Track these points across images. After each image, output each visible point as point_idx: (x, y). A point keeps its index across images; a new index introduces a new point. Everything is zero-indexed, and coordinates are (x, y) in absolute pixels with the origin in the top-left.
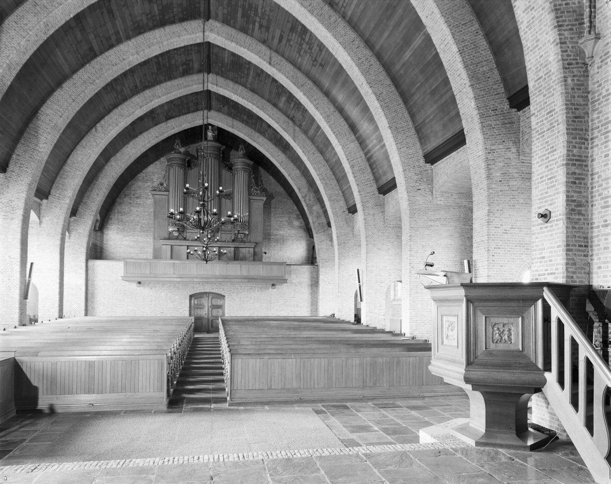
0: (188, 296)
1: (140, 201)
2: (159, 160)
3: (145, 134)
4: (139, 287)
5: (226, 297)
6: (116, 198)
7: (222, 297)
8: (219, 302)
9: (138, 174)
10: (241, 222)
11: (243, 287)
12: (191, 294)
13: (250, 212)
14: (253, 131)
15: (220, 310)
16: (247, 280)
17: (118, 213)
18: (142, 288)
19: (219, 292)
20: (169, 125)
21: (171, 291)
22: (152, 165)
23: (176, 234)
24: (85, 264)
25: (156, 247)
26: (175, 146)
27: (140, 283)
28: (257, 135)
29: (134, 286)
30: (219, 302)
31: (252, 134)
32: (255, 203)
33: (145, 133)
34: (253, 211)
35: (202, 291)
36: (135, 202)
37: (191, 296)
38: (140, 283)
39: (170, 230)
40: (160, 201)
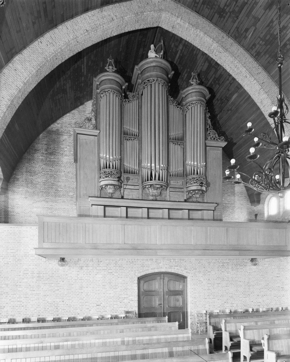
0: (136, 279)
1: (54, 158)
2: (77, 109)
3: (69, 24)
4: (62, 265)
5: (189, 279)
6: (24, 153)
7: (182, 278)
8: (178, 286)
9: (51, 124)
10: (197, 174)
11: (212, 264)
12: (139, 275)
13: (206, 162)
14: (225, 35)
15: (180, 298)
16: (237, 252)
17: (26, 172)
18: (66, 268)
19: (179, 272)
20: (105, 13)
21: (110, 271)
22: (68, 114)
23: (110, 190)
24: (136, 285)
25: (82, 208)
26: (106, 68)
27: (63, 259)
28: (230, 41)
29: (54, 264)
30: (178, 286)
31: (224, 40)
32: (211, 151)
33: (69, 22)
34: (209, 160)
35: (156, 271)
36: (48, 159)
37: (139, 279)
38: (63, 259)
39: (103, 183)
40: (86, 143)
